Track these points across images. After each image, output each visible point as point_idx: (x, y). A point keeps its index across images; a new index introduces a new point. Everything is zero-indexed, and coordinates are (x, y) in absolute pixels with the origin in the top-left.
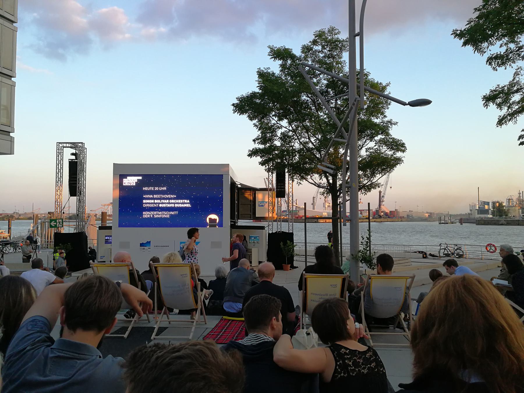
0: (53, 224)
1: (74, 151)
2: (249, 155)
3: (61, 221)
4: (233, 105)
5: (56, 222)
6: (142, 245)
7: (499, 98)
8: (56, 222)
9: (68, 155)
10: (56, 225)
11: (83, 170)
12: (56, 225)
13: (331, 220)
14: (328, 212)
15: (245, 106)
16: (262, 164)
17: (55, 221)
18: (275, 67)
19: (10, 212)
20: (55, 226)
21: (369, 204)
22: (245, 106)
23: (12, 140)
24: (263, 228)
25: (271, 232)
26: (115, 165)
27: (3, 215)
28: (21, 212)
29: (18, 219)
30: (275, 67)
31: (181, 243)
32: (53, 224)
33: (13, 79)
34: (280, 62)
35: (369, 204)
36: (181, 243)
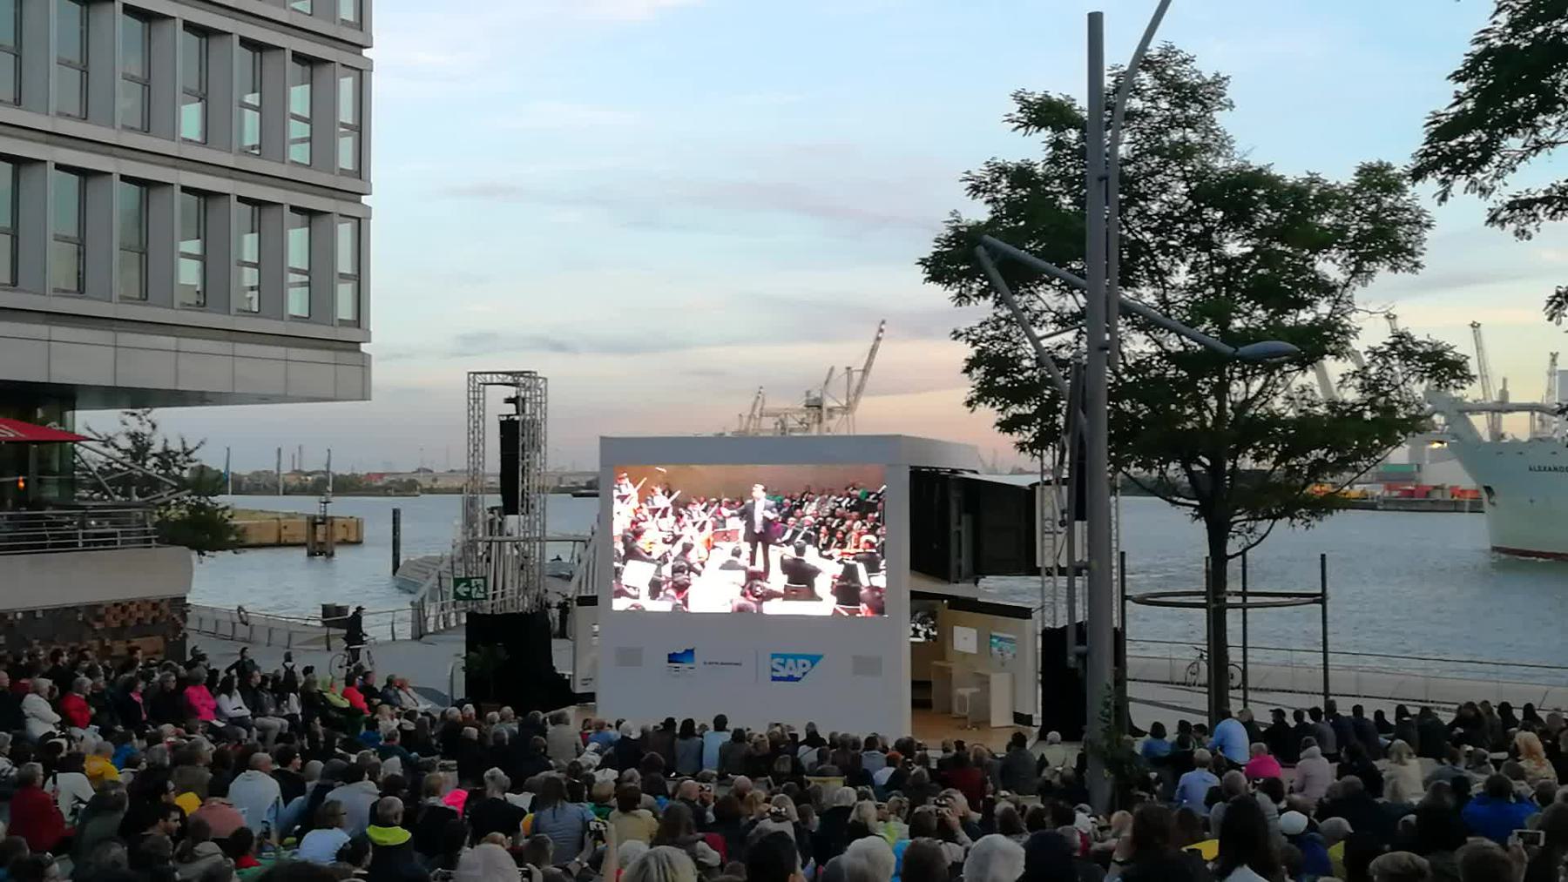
0: (462, 589)
1: (511, 392)
2: (969, 403)
3: (481, 581)
4: (923, 262)
5: (469, 585)
6: (673, 658)
7: (410, 715)
8: (469, 585)
9: (497, 405)
10: (469, 593)
11: (536, 445)
12: (469, 593)
13: (1230, 600)
14: (1527, 414)
15: (956, 260)
16: (1008, 426)
17: (467, 580)
18: (1034, 148)
19: (405, 466)
20: (469, 596)
21: (1323, 556)
22: (956, 260)
23: (365, 363)
24: (1024, 613)
25: (1049, 625)
26: (602, 438)
27: (387, 479)
28: (438, 469)
29: (431, 491)
30: (1034, 148)
31: (774, 656)
32: (462, 589)
33: (365, 52)
34: (1046, 134)
35: (1323, 556)
36: (774, 656)
